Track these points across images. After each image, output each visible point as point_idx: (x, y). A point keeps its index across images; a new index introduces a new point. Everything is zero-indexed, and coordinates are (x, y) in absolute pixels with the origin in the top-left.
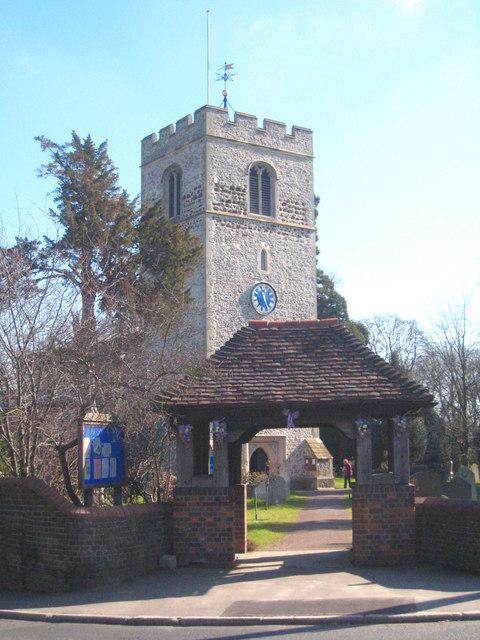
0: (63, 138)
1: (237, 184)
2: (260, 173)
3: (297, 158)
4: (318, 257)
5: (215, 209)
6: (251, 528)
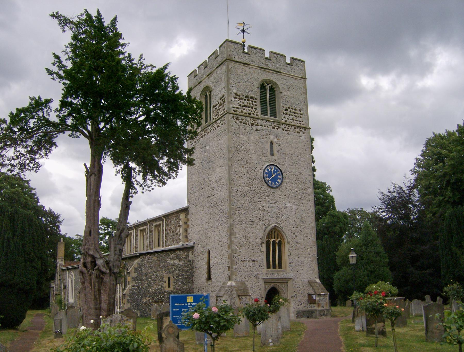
0: (74, 13)
1: (250, 94)
2: (268, 87)
3: (295, 78)
4: (315, 173)
5: (234, 111)
6: (423, 330)
